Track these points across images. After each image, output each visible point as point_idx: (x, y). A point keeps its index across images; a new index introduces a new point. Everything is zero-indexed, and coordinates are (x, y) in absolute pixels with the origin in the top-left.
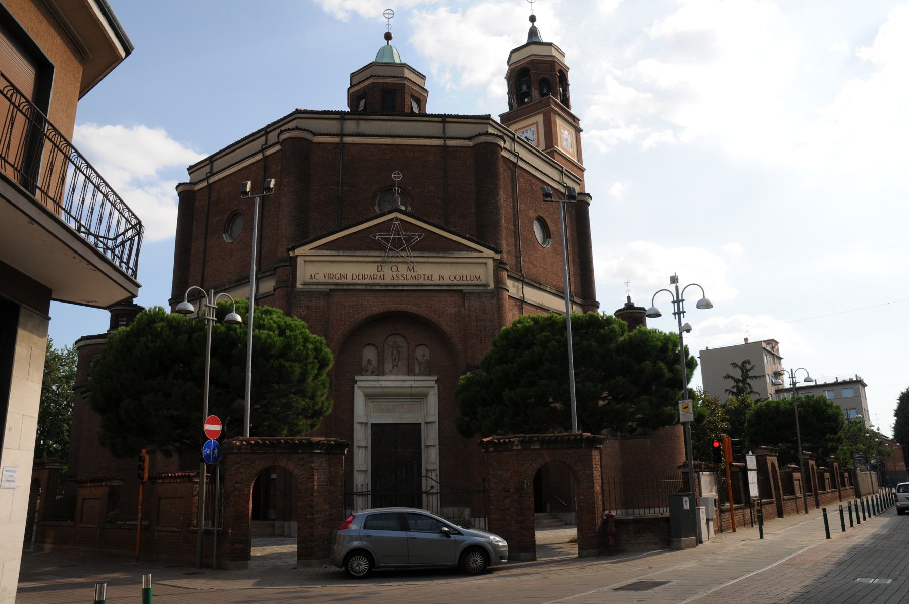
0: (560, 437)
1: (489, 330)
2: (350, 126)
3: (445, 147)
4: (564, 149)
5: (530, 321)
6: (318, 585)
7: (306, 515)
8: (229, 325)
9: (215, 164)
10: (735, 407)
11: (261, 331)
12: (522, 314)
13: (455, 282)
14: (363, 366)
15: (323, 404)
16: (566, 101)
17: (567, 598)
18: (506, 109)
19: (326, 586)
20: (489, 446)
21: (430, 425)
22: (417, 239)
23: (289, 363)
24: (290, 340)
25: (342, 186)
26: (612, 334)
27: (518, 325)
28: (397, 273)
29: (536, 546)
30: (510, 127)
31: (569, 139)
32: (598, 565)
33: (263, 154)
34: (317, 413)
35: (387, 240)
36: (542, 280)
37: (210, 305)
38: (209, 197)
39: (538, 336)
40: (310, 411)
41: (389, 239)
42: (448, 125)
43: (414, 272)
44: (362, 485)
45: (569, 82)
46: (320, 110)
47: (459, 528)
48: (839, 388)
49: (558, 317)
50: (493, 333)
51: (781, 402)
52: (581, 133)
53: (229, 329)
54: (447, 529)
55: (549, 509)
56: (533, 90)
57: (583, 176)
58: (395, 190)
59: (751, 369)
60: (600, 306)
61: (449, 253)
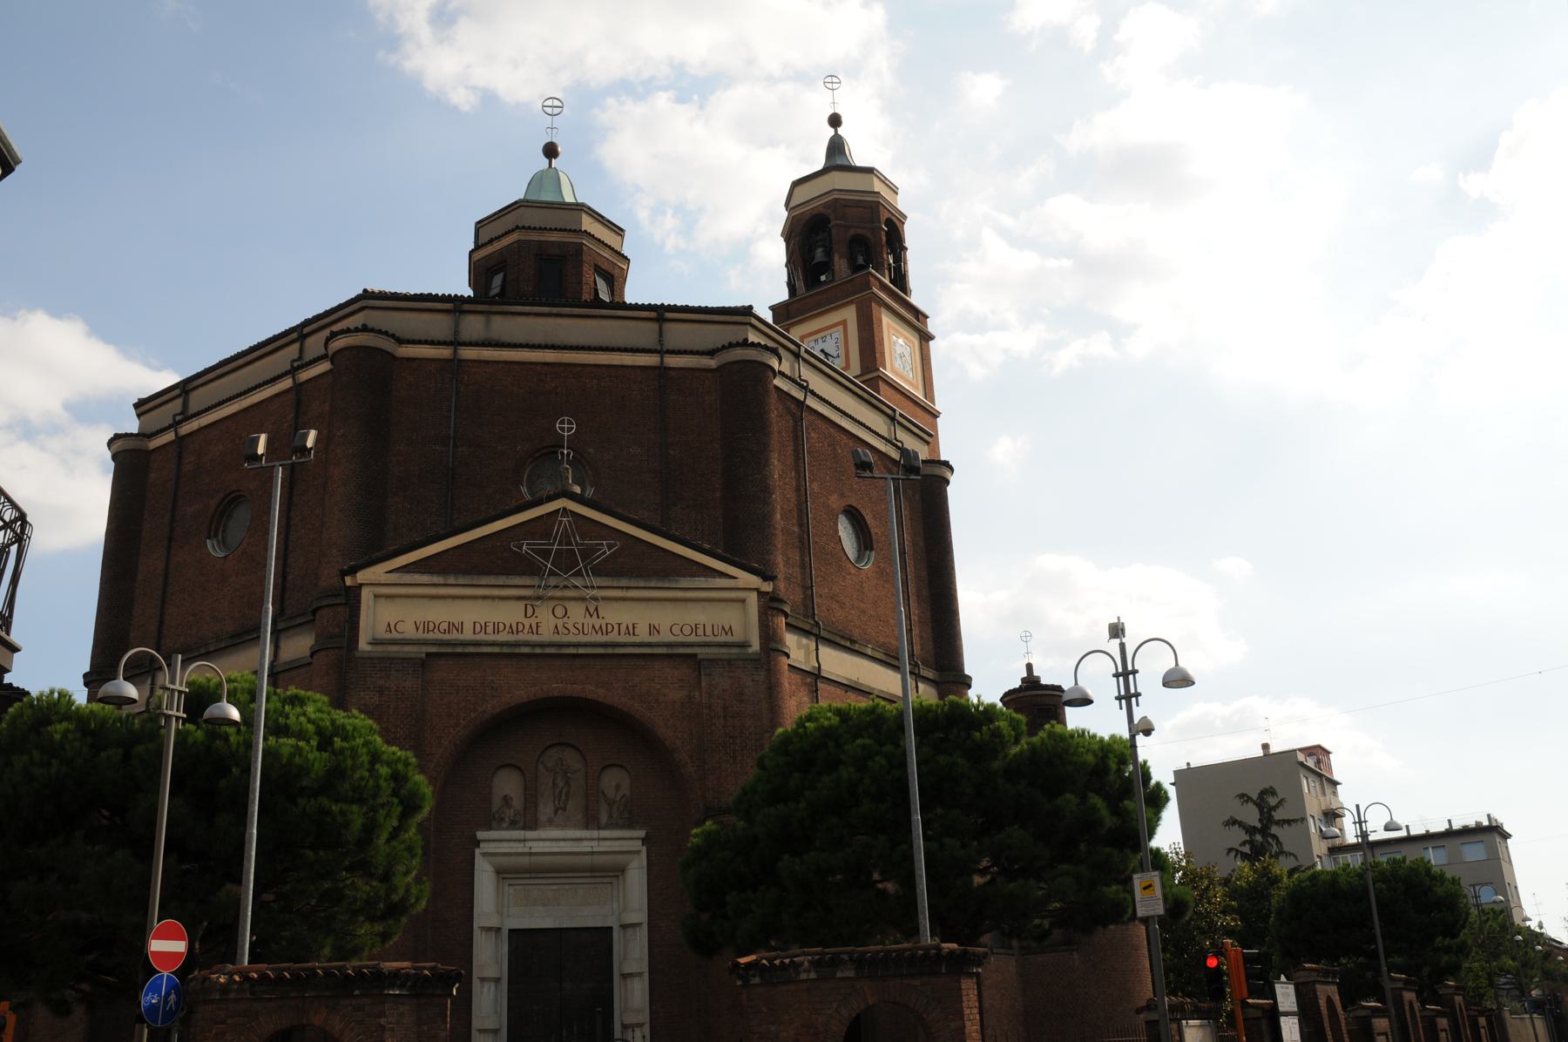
0: (895, 951)
1: (750, 734)
2: (473, 326)
3: (662, 370)
4: (897, 374)
10: (1248, 883)
11: (281, 740)
13: (681, 639)
15: (407, 891)
16: (900, 279)
18: (782, 295)
21: (630, 931)
22: (605, 553)
24: (341, 758)
26: (996, 740)
27: (807, 724)
28: (565, 619)
30: (792, 330)
31: (907, 355)
34: (395, 910)
35: (545, 554)
36: (856, 634)
37: (172, 687)
38: (179, 464)
40: (382, 906)
41: (548, 552)
42: (667, 326)
43: (598, 617)
45: (907, 244)
48: (1458, 841)
49: (889, 707)
51: (1340, 872)
53: (213, 735)
56: (836, 258)
58: (562, 453)
59: (1277, 806)
61: (670, 580)
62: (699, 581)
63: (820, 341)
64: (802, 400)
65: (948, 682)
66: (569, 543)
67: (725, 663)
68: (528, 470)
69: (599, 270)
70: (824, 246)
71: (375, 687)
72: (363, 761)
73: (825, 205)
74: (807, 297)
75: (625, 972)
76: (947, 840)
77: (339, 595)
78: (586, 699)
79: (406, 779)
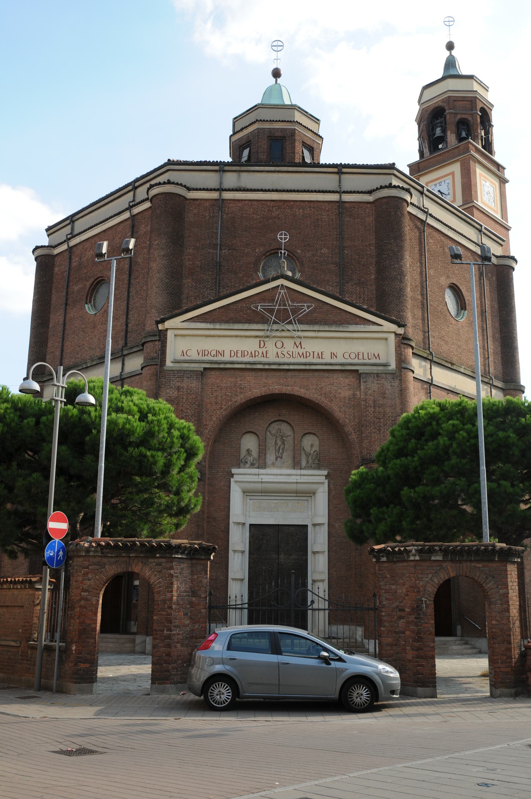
0: (467, 546)
1: (389, 417)
3: (341, 203)
4: (485, 204)
5: (436, 407)
6: (170, 716)
7: (163, 631)
8: (83, 408)
9: (77, 224)
11: (118, 415)
12: (430, 398)
13: (350, 361)
14: (241, 457)
15: (189, 500)
16: (488, 145)
17: (467, 753)
18: (416, 157)
19: (179, 719)
20: (381, 555)
21: (318, 527)
22: (305, 311)
23: (151, 452)
24: (152, 425)
25: (221, 249)
27: (420, 411)
28: (283, 349)
29: (437, 680)
30: (421, 179)
32: (513, 710)
33: (130, 212)
34: (183, 511)
35: (271, 311)
36: (454, 361)
37: (58, 384)
38: (70, 262)
39: (444, 425)
40: (175, 508)
42: (343, 177)
43: (301, 348)
44: (236, 597)
45: (494, 123)
46: (196, 161)
47: (341, 653)
49: (470, 402)
50: (394, 421)
52: (506, 184)
53: (82, 412)
54: (326, 654)
55: (459, 632)
56: (449, 133)
57: (507, 236)
58: (281, 253)
60: (526, 391)
62: (361, 327)
63: (438, 185)
64: (425, 220)
65: (510, 389)
66: (285, 305)
67: (375, 375)
68: (262, 263)
69: (305, 145)
70: (442, 126)
71: (176, 387)
72: (164, 428)
73: (443, 101)
74: (430, 159)
75: (315, 550)
76: (503, 482)
77: (156, 335)
78: (294, 395)
79: (188, 438)
